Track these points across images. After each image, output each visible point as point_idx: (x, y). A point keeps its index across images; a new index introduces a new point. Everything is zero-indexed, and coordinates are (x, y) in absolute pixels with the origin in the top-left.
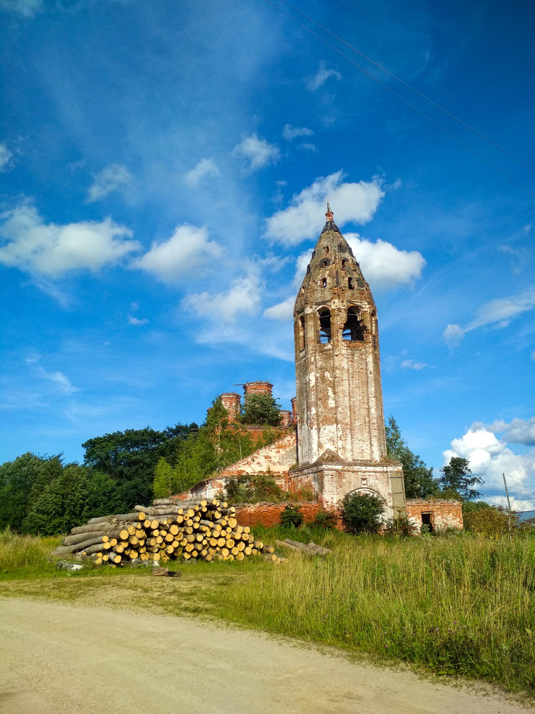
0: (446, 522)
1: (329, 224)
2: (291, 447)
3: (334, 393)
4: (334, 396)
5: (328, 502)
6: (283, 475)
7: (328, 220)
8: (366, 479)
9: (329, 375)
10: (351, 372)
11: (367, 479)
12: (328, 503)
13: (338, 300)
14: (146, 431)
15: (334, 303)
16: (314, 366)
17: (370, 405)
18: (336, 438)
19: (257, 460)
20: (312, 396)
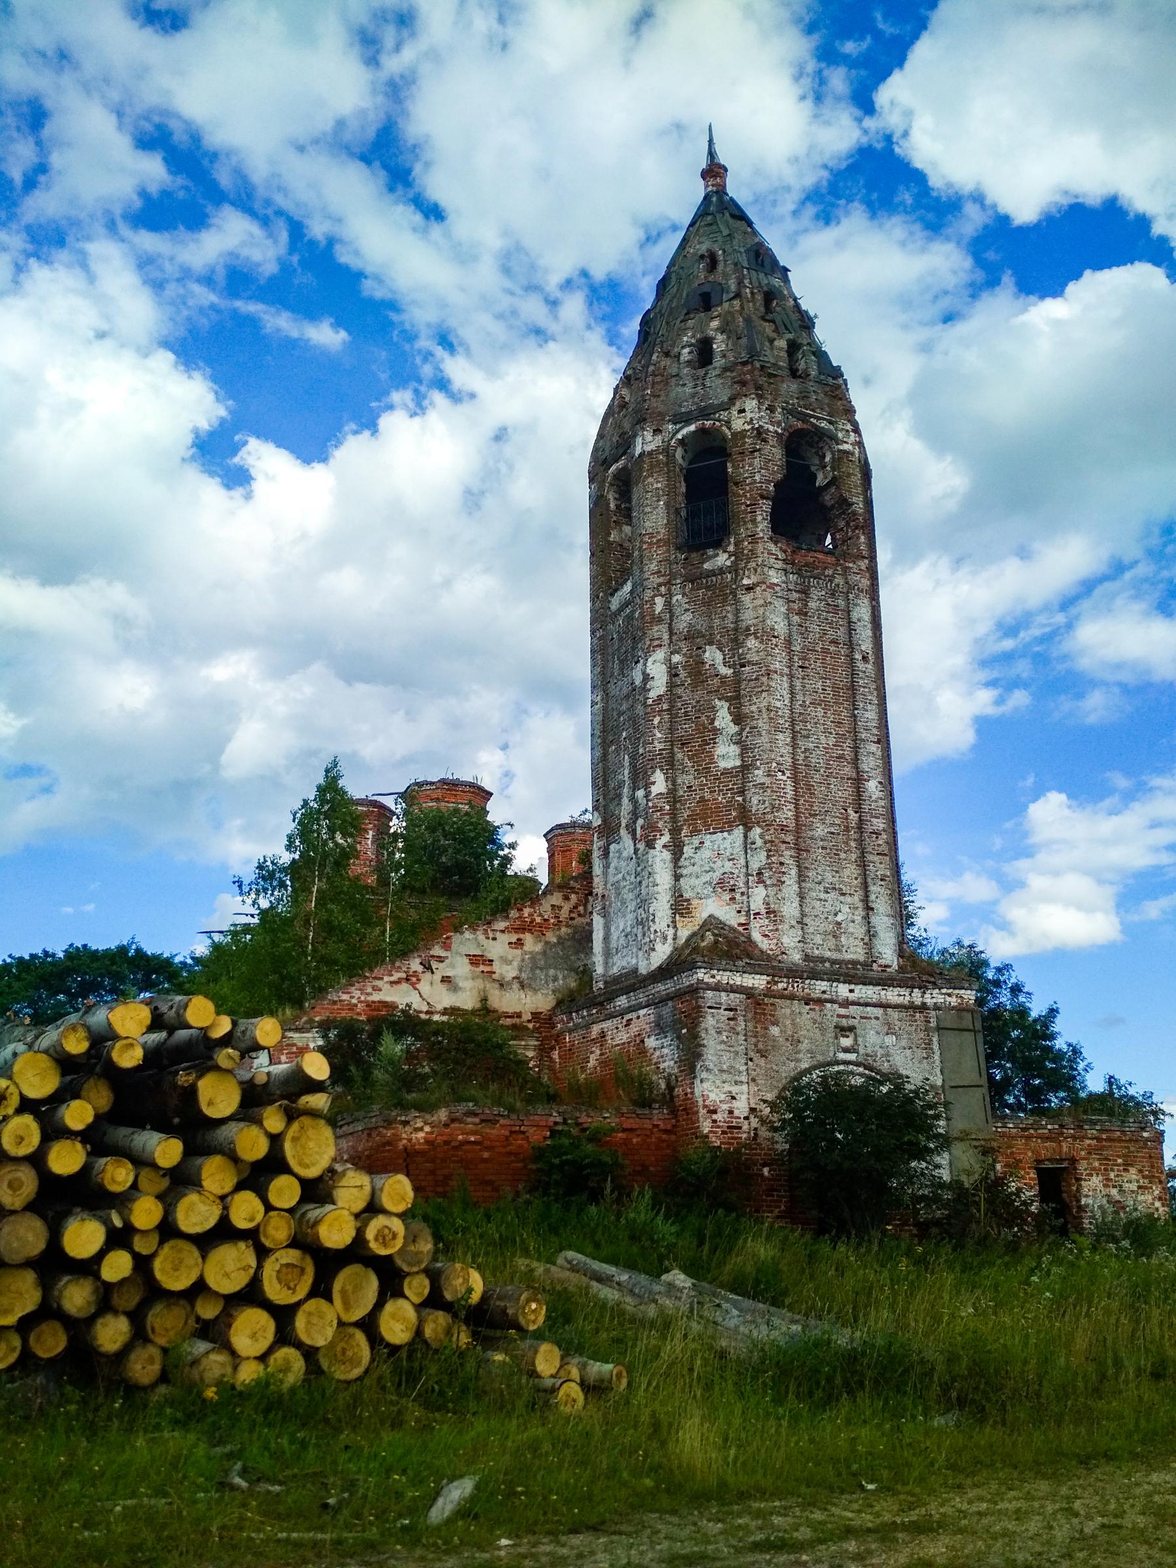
0: (1118, 1198)
1: (714, 199)
2: (564, 929)
3: (738, 719)
4: (735, 729)
5: (715, 1112)
6: (530, 1026)
7: (710, 189)
8: (852, 1029)
9: (719, 657)
10: (798, 648)
11: (858, 1031)
12: (715, 1117)
13: (755, 402)
14: (122, 950)
15: (742, 411)
16: (664, 628)
17: (864, 767)
18: (742, 879)
19: (441, 970)
20: (656, 731)
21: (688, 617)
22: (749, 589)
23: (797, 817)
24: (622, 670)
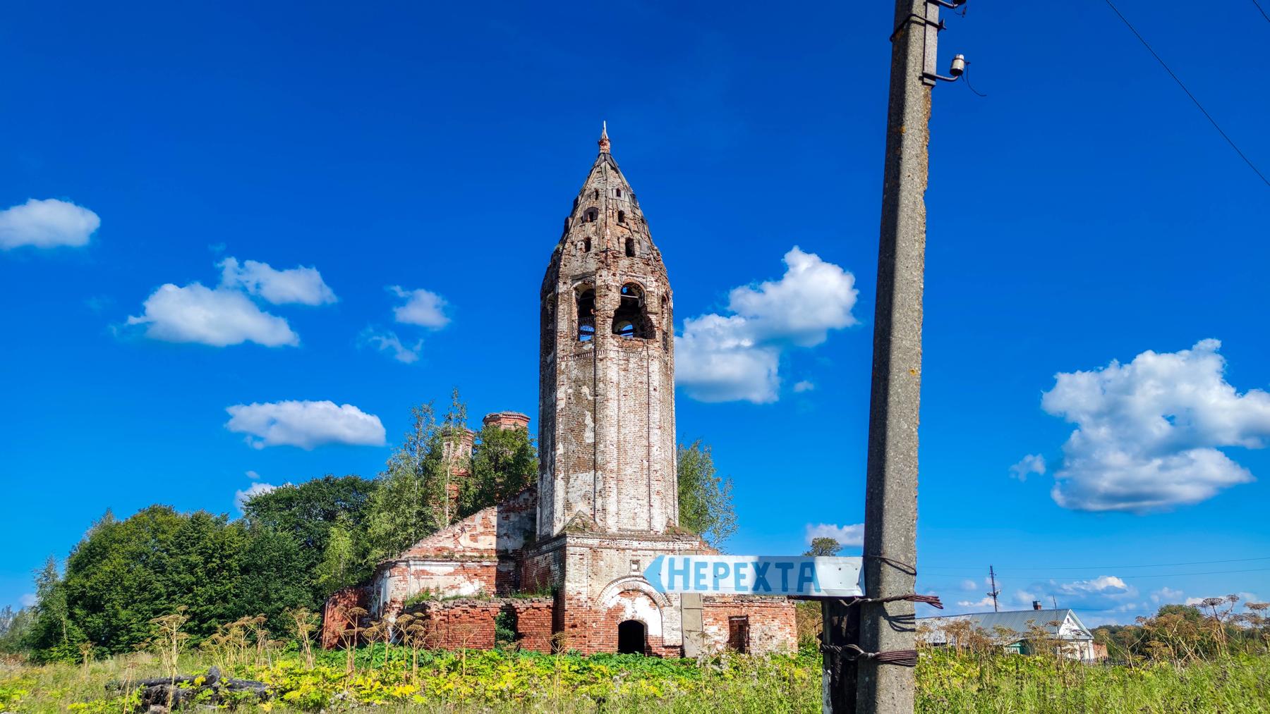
15: (601, 276)
23: (618, 465)
24: (550, 393)
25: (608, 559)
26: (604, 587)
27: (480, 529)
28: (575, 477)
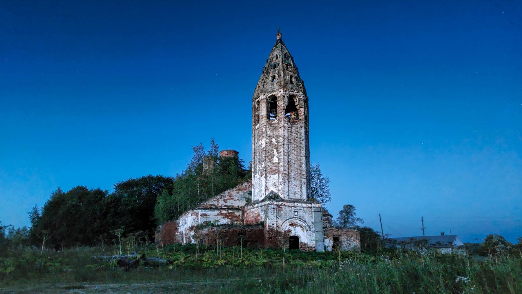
0: (349, 243)
3: (278, 153)
8: (297, 211)
18: (278, 184)
20: (263, 154)
21: (269, 132)
22: (280, 127)
25: (285, 211)
26: (283, 222)
27: (228, 197)
28: (270, 176)
